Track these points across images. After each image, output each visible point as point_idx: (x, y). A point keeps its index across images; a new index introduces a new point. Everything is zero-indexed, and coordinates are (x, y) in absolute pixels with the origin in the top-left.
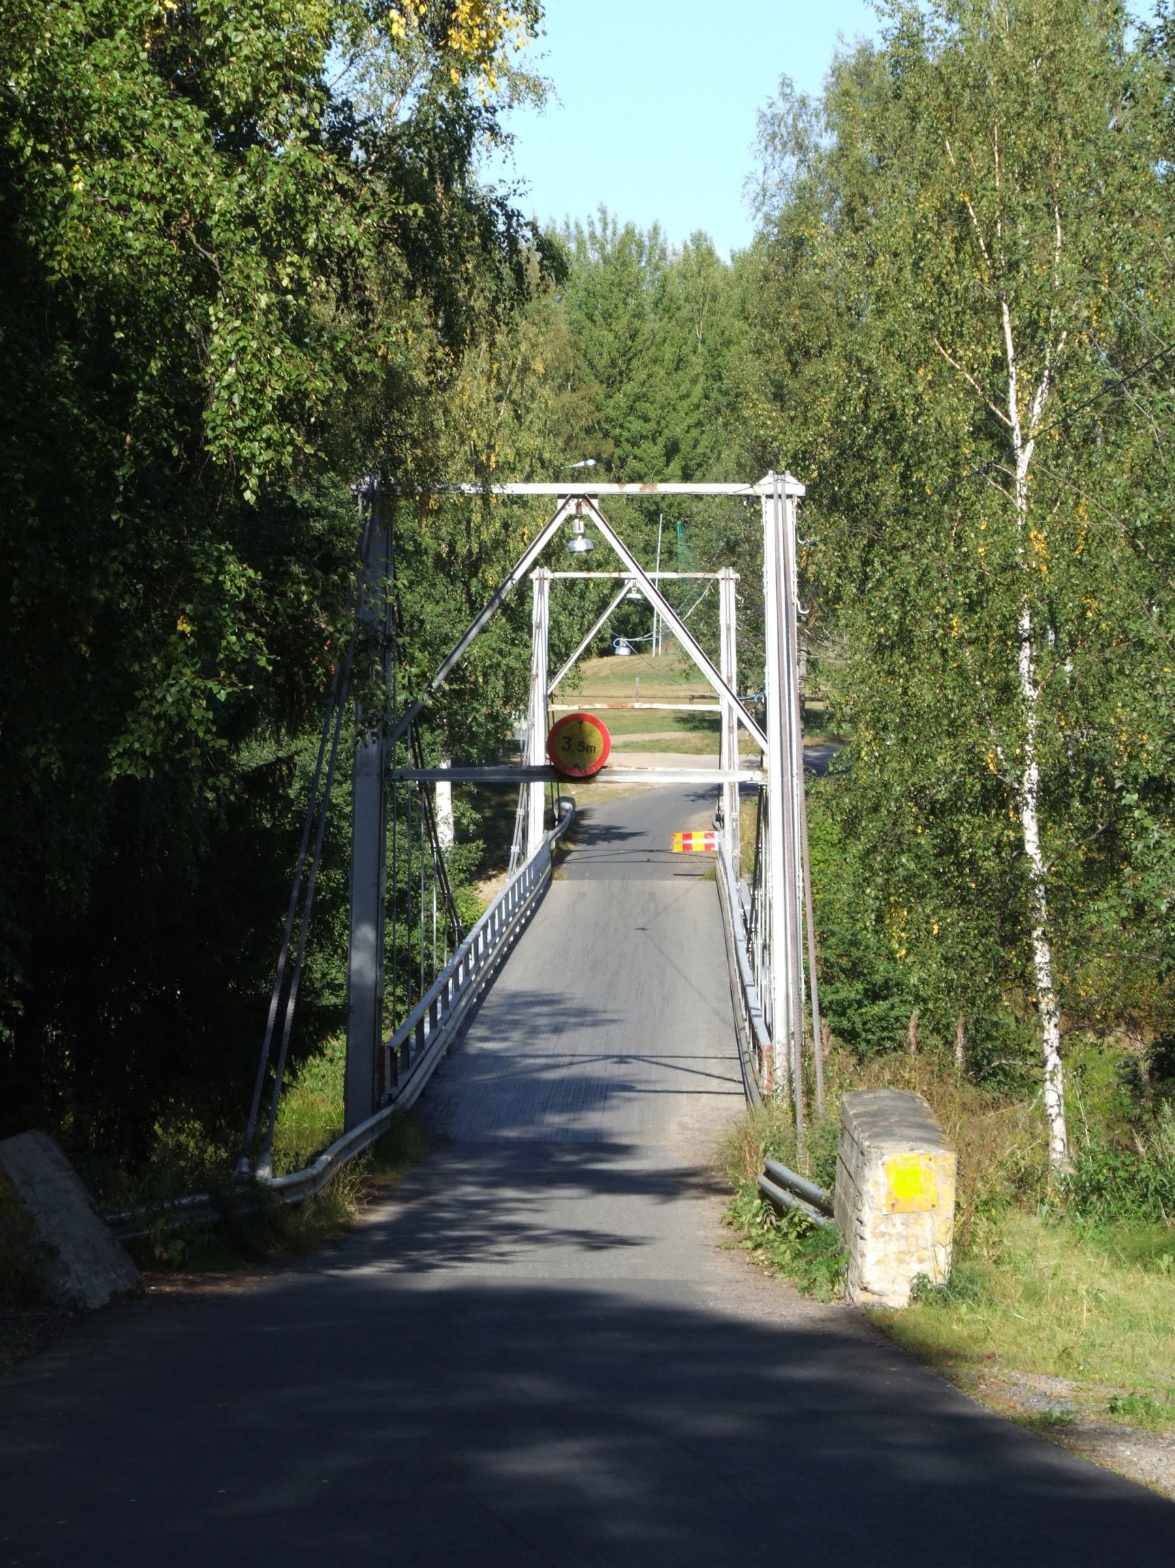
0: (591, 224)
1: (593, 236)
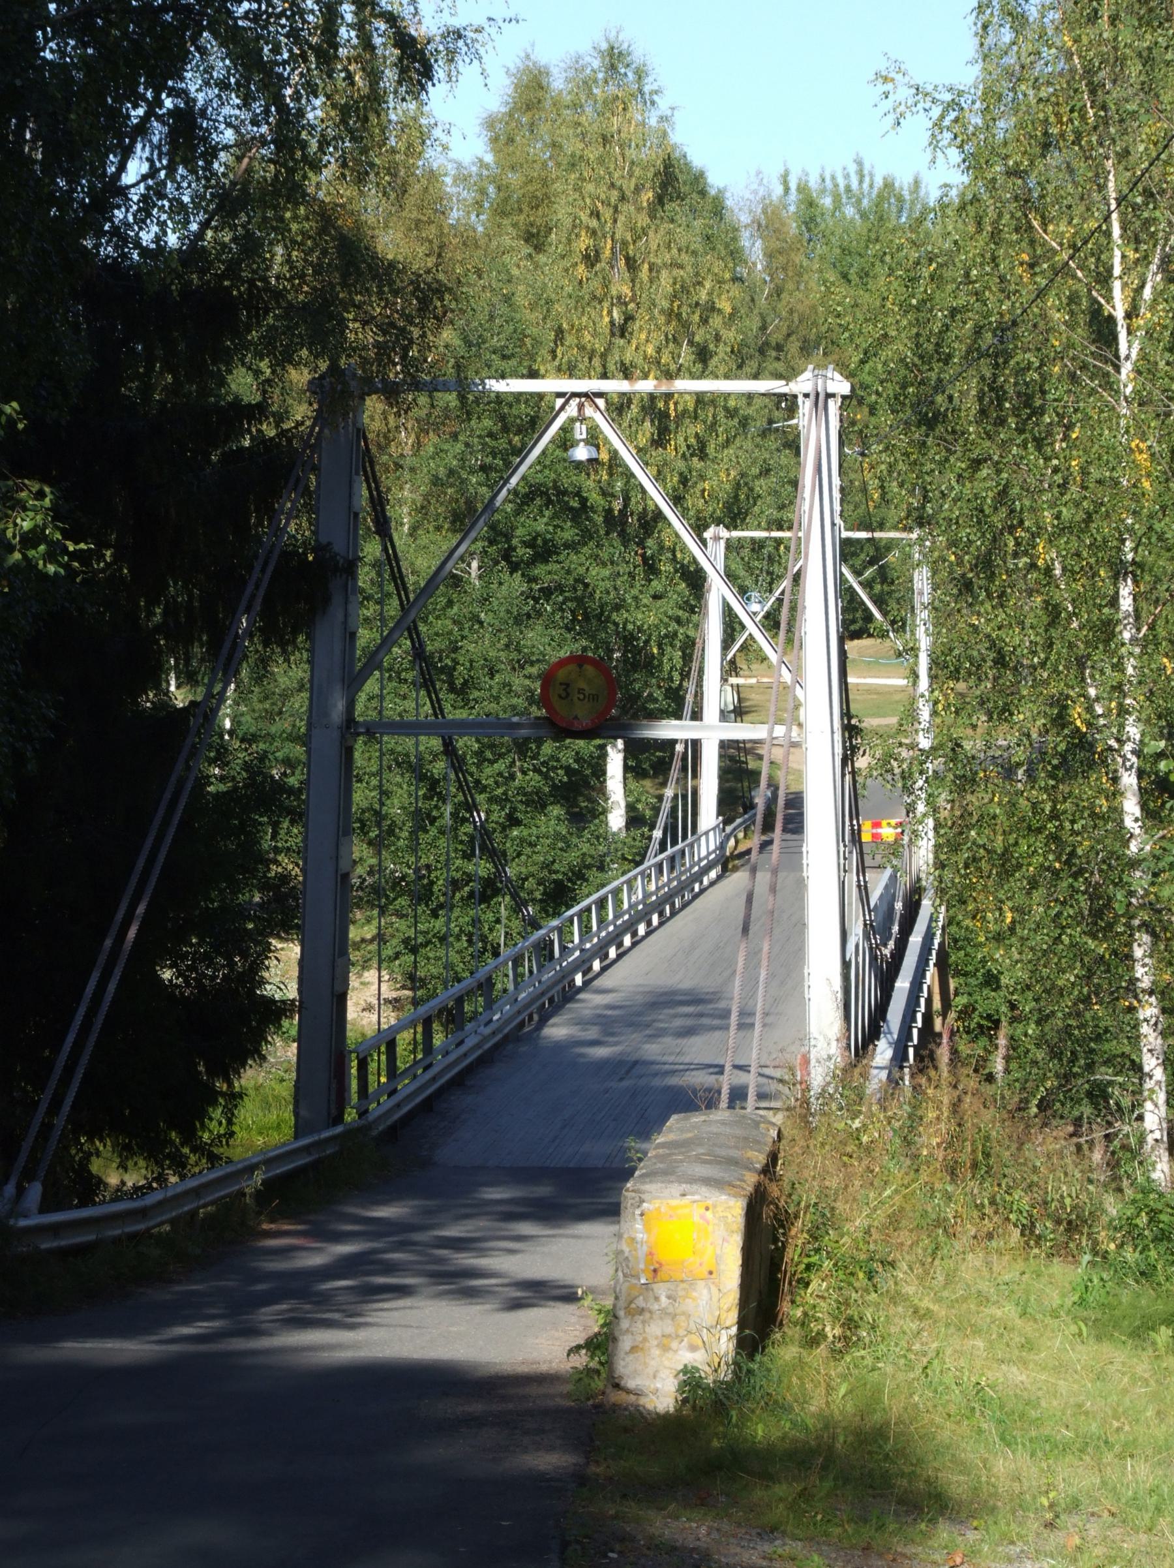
0: (847, 176)
1: (848, 189)
